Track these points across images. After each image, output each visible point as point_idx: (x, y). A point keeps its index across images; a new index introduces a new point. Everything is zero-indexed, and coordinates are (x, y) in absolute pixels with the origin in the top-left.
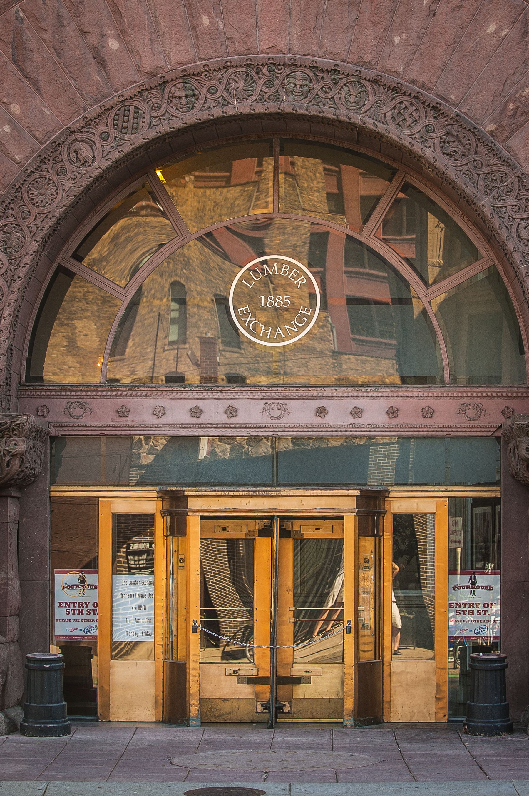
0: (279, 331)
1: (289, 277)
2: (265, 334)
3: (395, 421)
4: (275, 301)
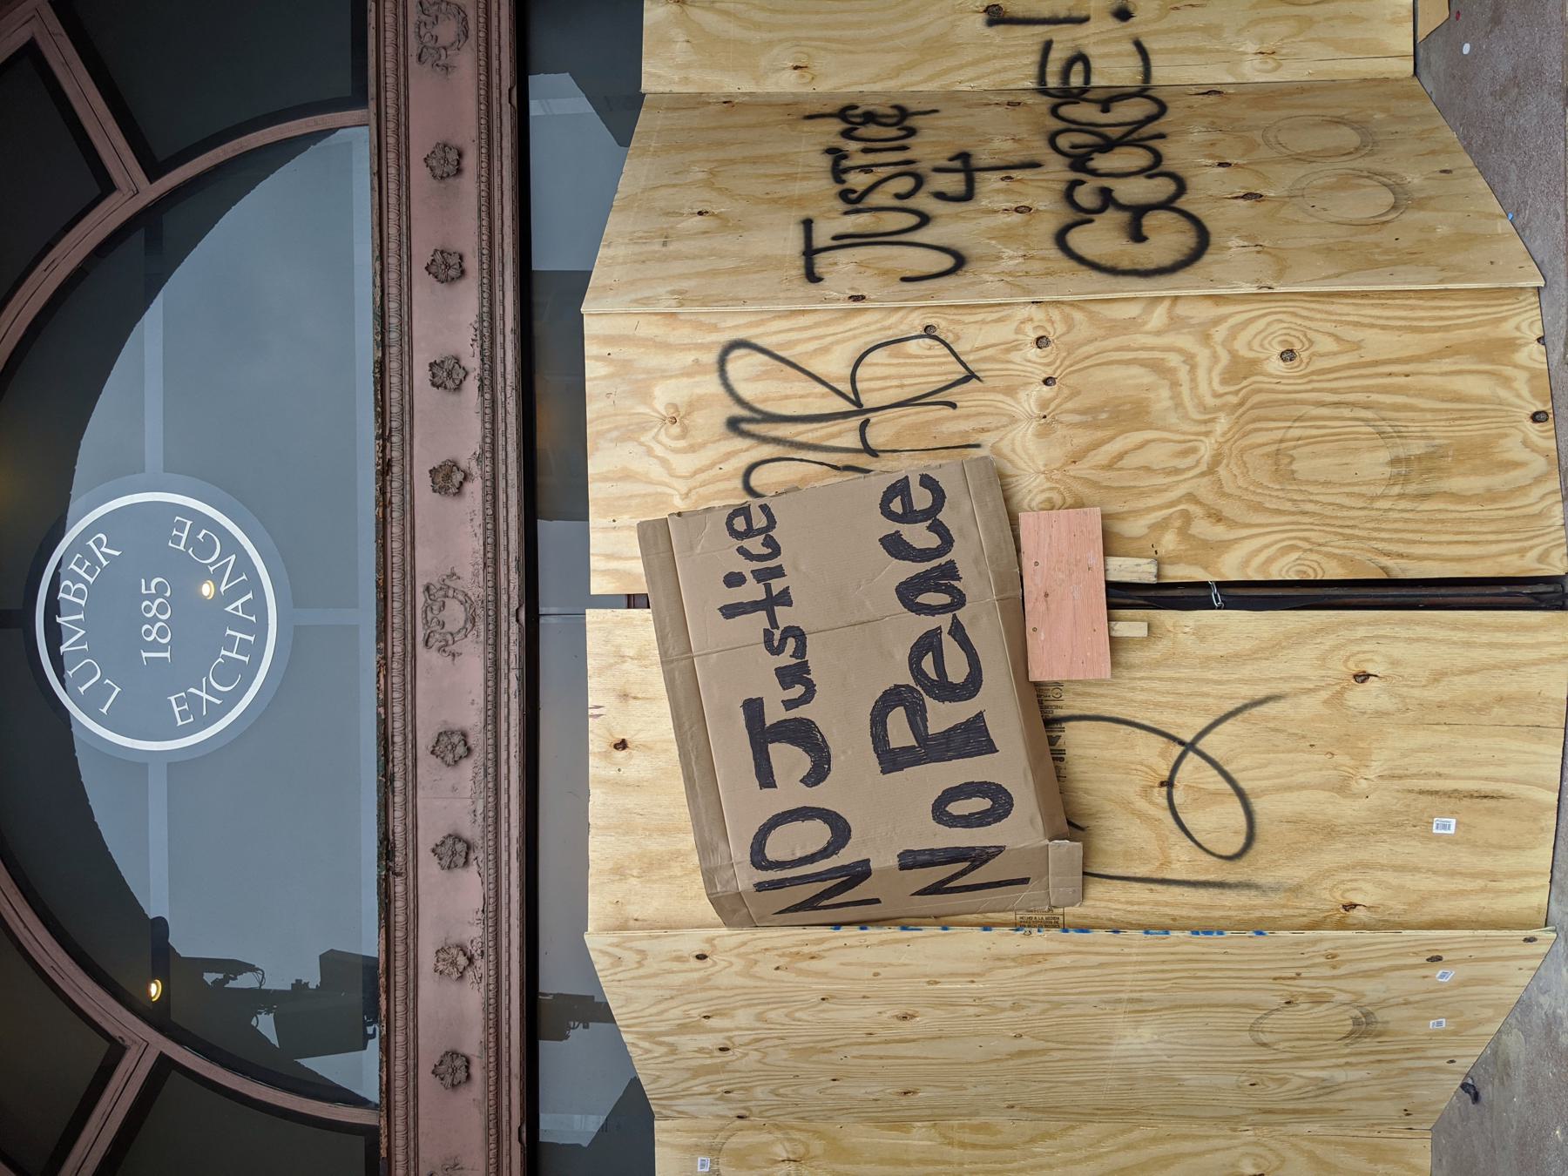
0: (236, 609)
1: (91, 580)
2: (244, 647)
3: (472, 264)
4: (154, 620)
